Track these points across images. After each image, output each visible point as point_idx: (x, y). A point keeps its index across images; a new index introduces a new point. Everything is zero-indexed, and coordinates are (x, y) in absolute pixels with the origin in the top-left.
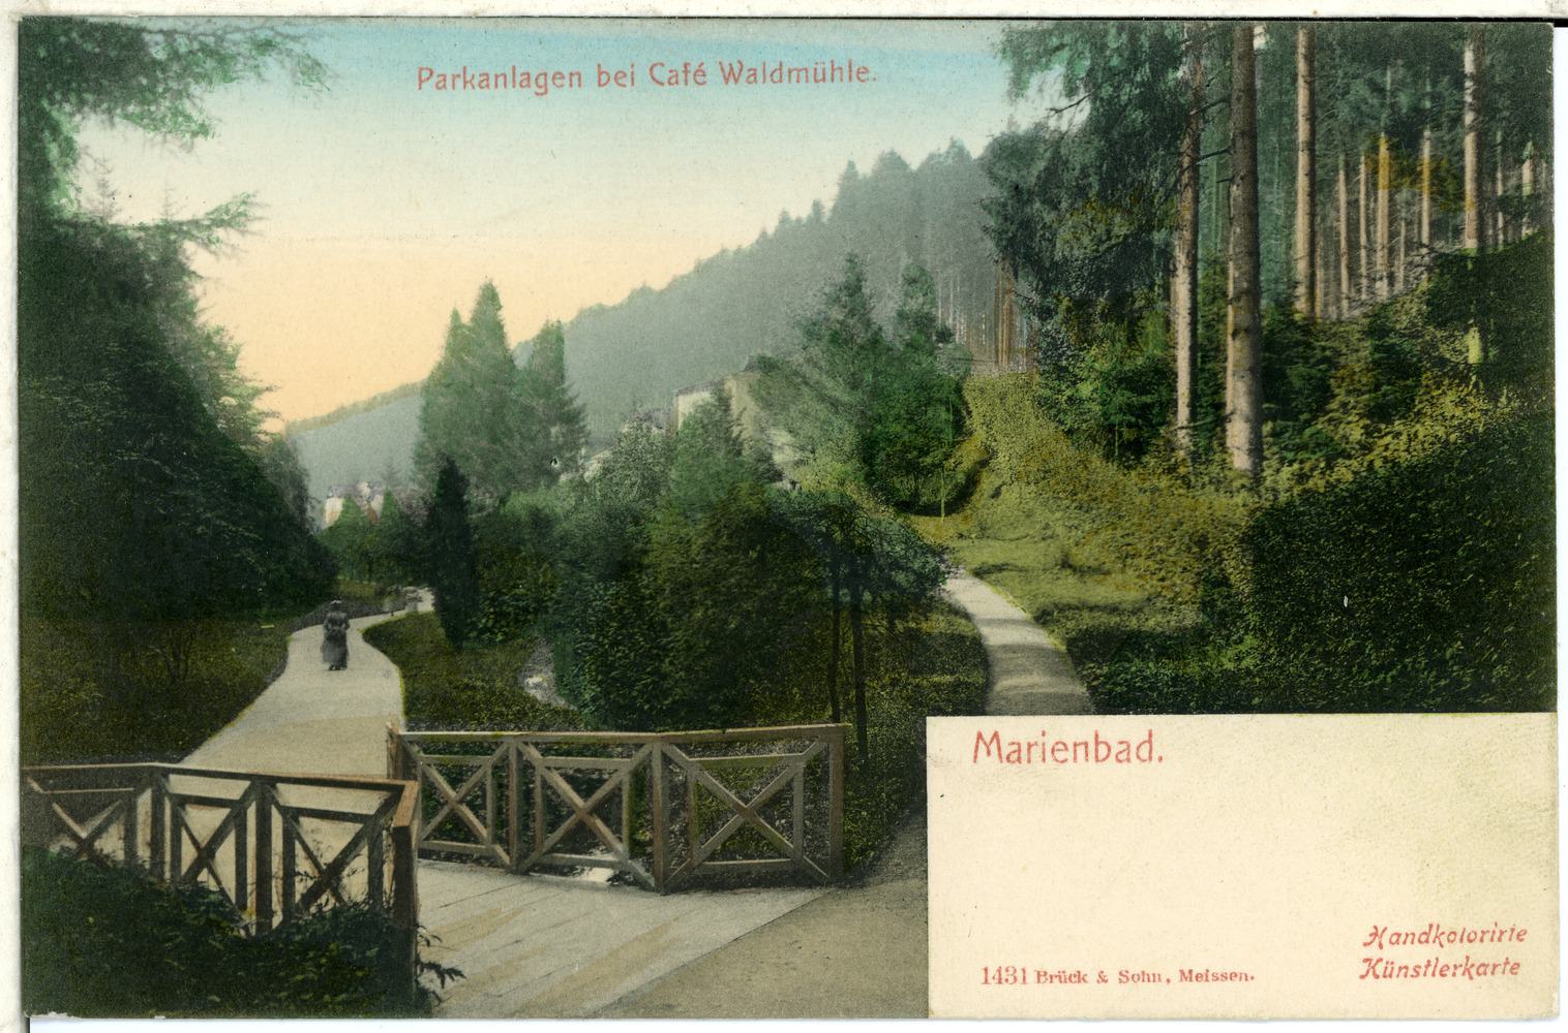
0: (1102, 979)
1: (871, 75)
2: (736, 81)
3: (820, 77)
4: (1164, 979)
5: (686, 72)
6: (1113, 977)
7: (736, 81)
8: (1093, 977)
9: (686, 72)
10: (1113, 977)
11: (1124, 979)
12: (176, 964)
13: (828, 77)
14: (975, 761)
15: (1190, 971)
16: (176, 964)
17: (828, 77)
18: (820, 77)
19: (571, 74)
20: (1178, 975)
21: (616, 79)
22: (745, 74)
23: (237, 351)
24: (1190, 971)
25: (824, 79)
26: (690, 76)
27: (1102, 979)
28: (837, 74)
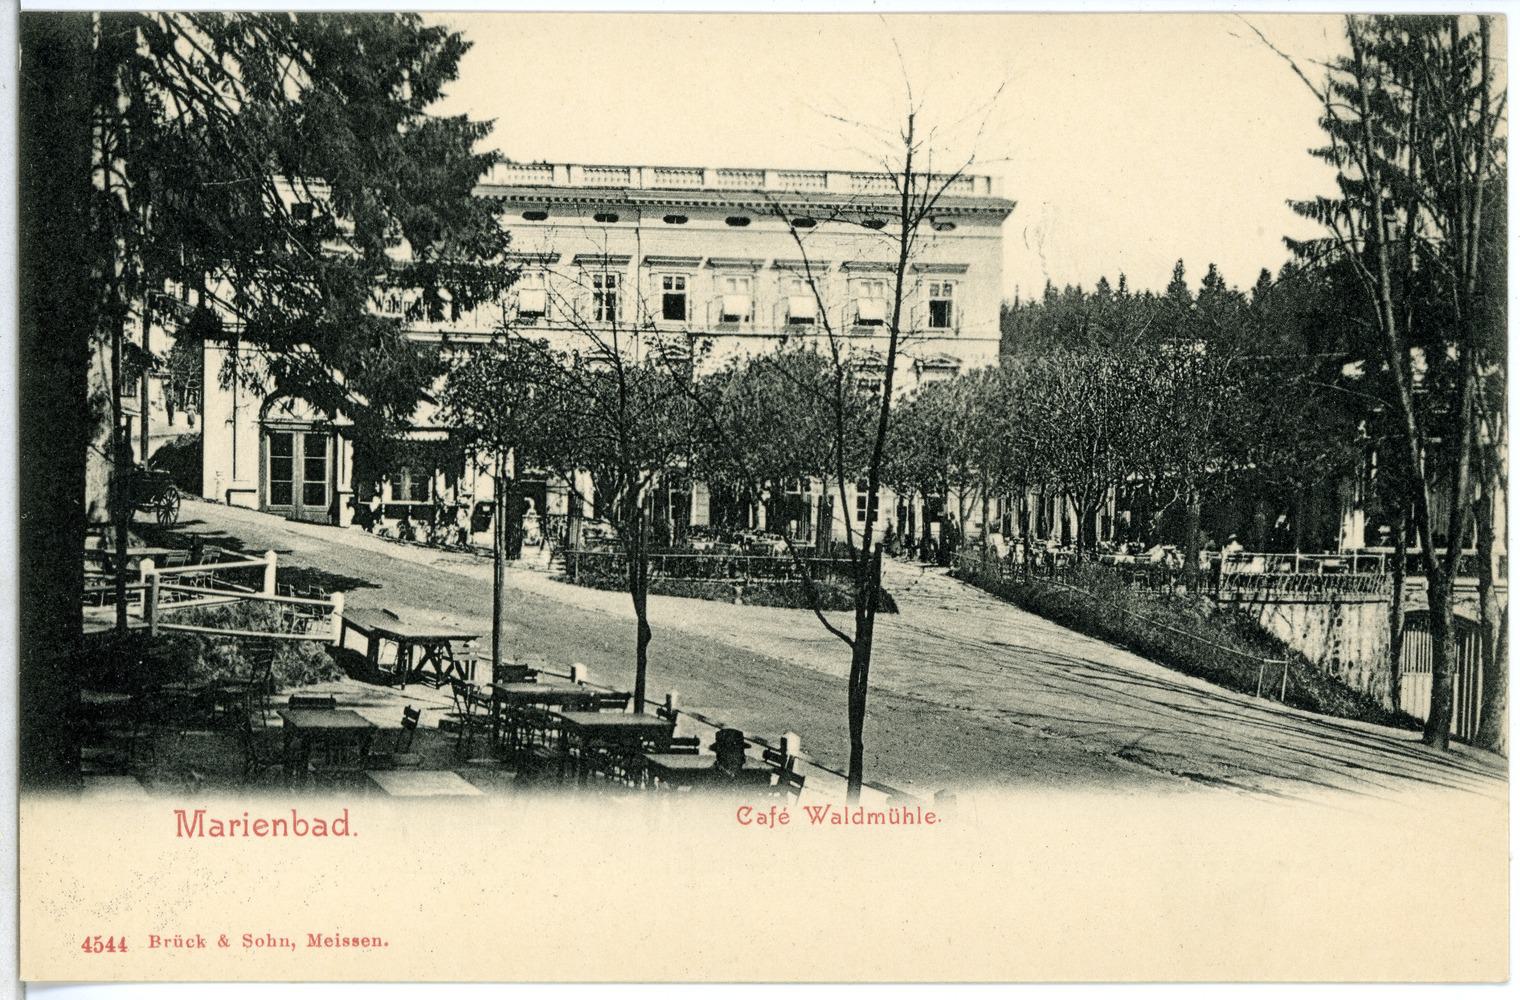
0: (223, 942)
1: (937, 818)
2: (821, 821)
3: (894, 819)
4: (383, 943)
5: (773, 814)
6: (236, 941)
7: (821, 821)
8: (212, 940)
9: (773, 814)
10: (236, 941)
11: (248, 943)
12: (337, 89)
13: (901, 820)
14: (377, 942)
15: (319, 936)
16: (337, 89)
17: (901, 820)
18: (894, 819)
19: (276, 823)
20: (307, 940)
21: (255, 829)
22: (829, 816)
23: (1503, 460)
24: (319, 936)
25: (898, 822)
26: (776, 817)
27: (223, 942)
28: (909, 819)
